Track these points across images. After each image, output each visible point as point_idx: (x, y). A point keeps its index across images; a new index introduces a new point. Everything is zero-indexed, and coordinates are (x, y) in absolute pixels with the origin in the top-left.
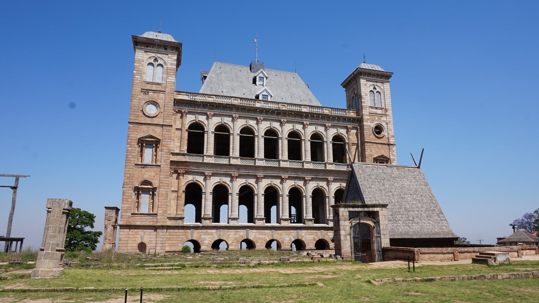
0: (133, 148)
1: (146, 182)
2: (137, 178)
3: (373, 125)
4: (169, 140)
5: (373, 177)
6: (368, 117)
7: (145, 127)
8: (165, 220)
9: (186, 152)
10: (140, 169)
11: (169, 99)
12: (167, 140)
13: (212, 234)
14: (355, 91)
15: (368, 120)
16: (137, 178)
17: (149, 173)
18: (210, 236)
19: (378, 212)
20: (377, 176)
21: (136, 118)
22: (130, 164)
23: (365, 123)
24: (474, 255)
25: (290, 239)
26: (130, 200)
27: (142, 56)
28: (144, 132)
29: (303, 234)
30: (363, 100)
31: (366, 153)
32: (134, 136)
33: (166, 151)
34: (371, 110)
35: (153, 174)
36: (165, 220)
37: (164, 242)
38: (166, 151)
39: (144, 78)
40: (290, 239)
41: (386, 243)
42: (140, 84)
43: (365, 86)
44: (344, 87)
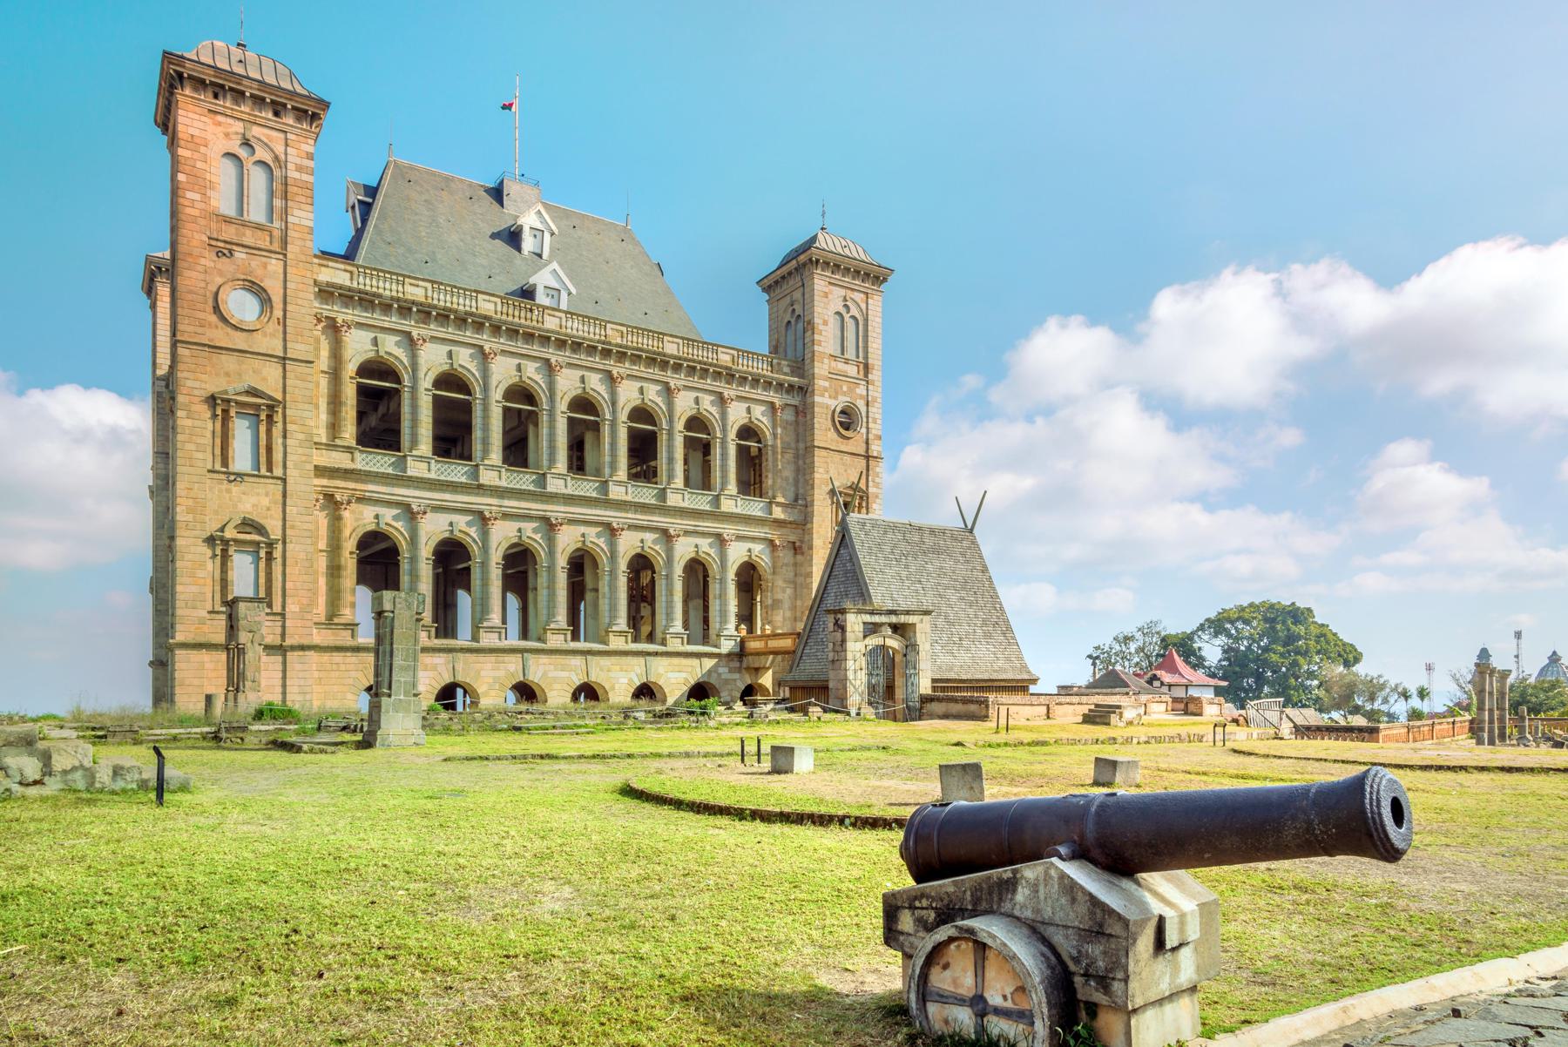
0: (197, 423)
1: (249, 525)
2: (216, 512)
3: (839, 403)
4: (306, 406)
5: (887, 549)
6: (827, 384)
7: (229, 362)
8: (306, 631)
9: (353, 443)
10: (225, 485)
11: (299, 279)
12: (300, 406)
13: (434, 668)
14: (798, 308)
15: (826, 389)
16: (216, 512)
17: (254, 500)
18: (431, 674)
19: (914, 625)
20: (895, 546)
21: (200, 330)
22: (191, 470)
23: (817, 399)
24: (1085, 709)
25: (631, 680)
26: (201, 574)
27: (201, 125)
28: (227, 374)
29: (661, 670)
30: (816, 337)
31: (816, 475)
32: (197, 384)
33: (301, 436)
34: (833, 364)
35: (265, 502)
36: (306, 631)
37: (308, 689)
38: (301, 436)
39: (213, 202)
40: (631, 680)
41: (925, 687)
42: (202, 222)
43: (827, 298)
44: (764, 290)
